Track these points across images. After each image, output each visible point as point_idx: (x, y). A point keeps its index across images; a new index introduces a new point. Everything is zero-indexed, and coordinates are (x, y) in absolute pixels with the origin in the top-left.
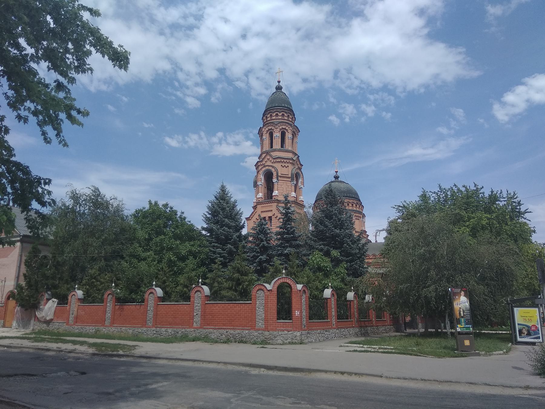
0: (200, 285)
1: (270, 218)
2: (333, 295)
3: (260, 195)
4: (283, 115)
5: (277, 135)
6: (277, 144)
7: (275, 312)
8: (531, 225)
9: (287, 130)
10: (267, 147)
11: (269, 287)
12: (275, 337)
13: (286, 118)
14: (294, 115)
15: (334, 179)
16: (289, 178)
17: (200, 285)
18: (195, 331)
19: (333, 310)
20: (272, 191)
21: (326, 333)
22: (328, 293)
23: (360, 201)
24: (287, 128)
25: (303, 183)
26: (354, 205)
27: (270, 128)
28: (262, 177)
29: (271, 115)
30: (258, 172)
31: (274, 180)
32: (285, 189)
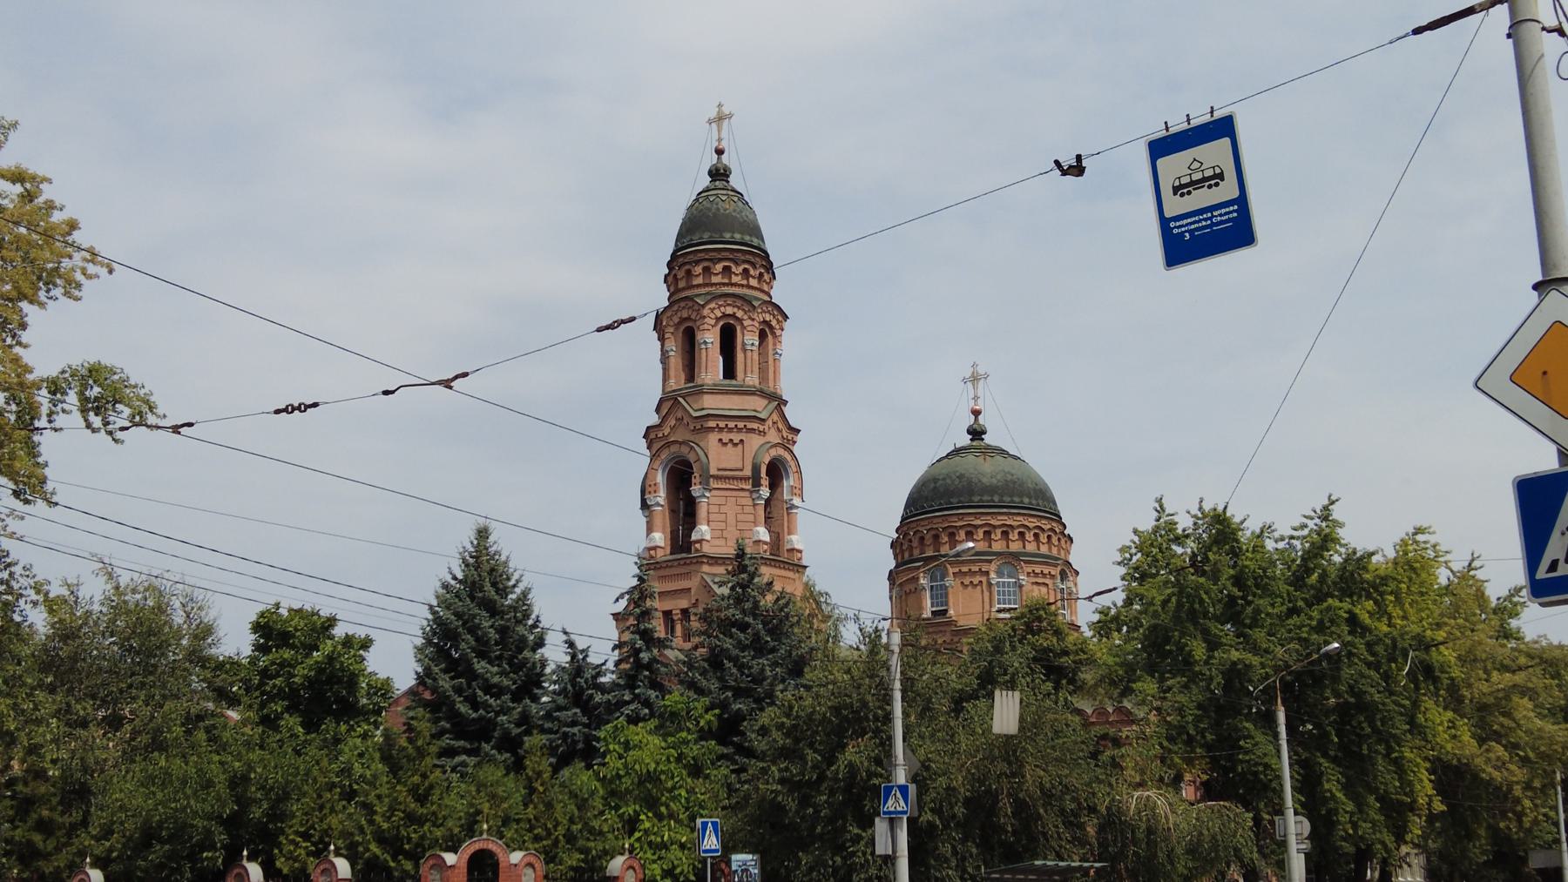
1: (685, 612)
5: (710, 338)
6: (712, 368)
8: (382, 675)
11: (450, 858)
15: (965, 440)
23: (1057, 518)
29: (707, 270)
31: (696, 490)
32: (731, 520)
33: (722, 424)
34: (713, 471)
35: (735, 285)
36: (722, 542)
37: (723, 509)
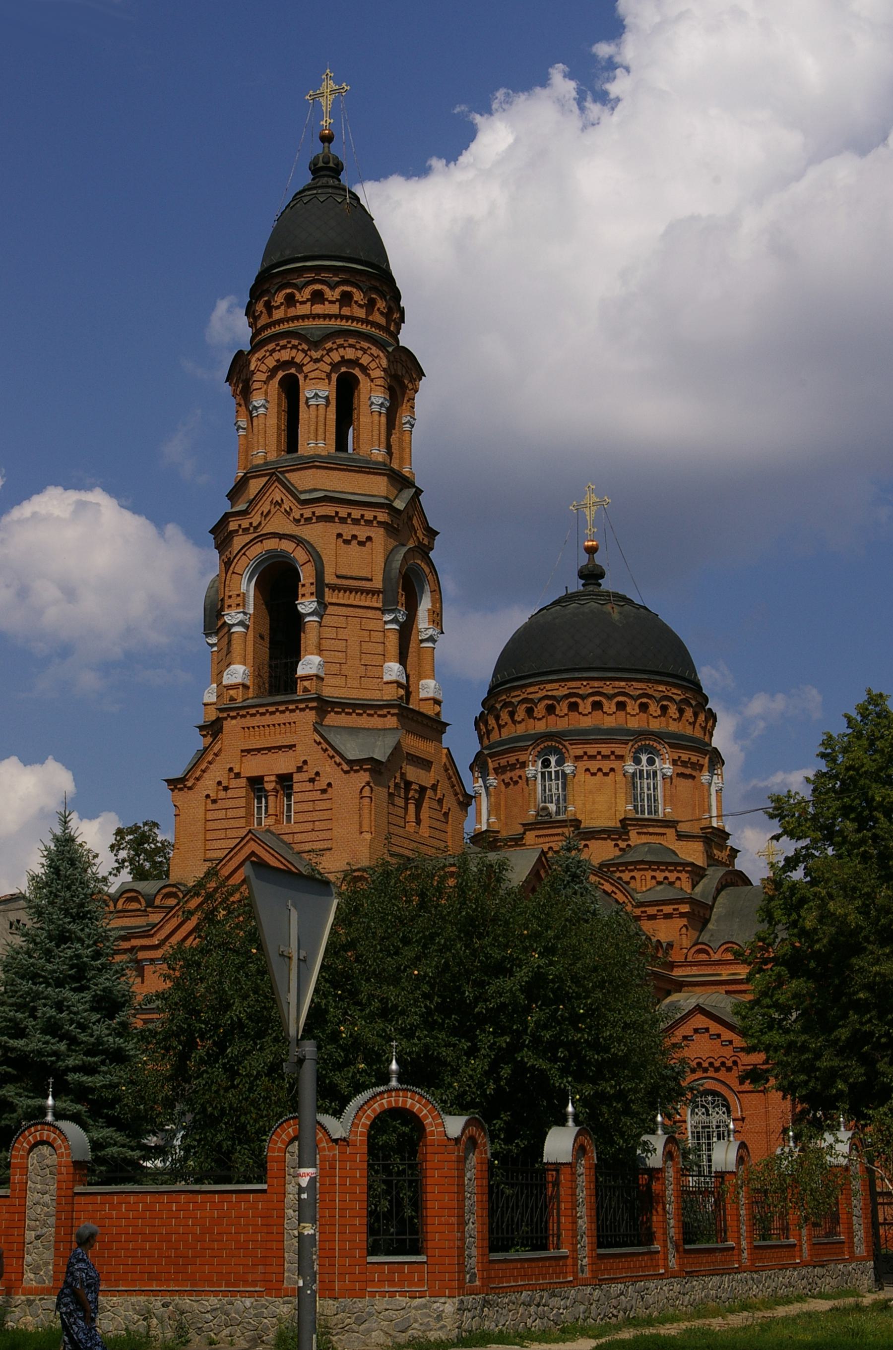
0: (50, 1118)
2: (580, 1150)
3: (237, 673)
4: (346, 299)
5: (317, 392)
6: (316, 440)
7: (360, 1222)
9: (364, 369)
10: (267, 448)
11: (336, 1127)
12: (360, 1321)
13: (361, 313)
15: (576, 585)
16: (373, 592)
17: (50, 1118)
18: (30, 1303)
19: (582, 1211)
20: (295, 655)
21: (554, 1301)
22: (559, 1144)
23: (696, 688)
24: (365, 360)
25: (436, 617)
26: (673, 710)
27: (285, 355)
28: (247, 587)
30: (227, 564)
31: (306, 605)
33: (343, 513)
34: (329, 578)
35: (353, 319)
36: (340, 681)
37: (342, 634)
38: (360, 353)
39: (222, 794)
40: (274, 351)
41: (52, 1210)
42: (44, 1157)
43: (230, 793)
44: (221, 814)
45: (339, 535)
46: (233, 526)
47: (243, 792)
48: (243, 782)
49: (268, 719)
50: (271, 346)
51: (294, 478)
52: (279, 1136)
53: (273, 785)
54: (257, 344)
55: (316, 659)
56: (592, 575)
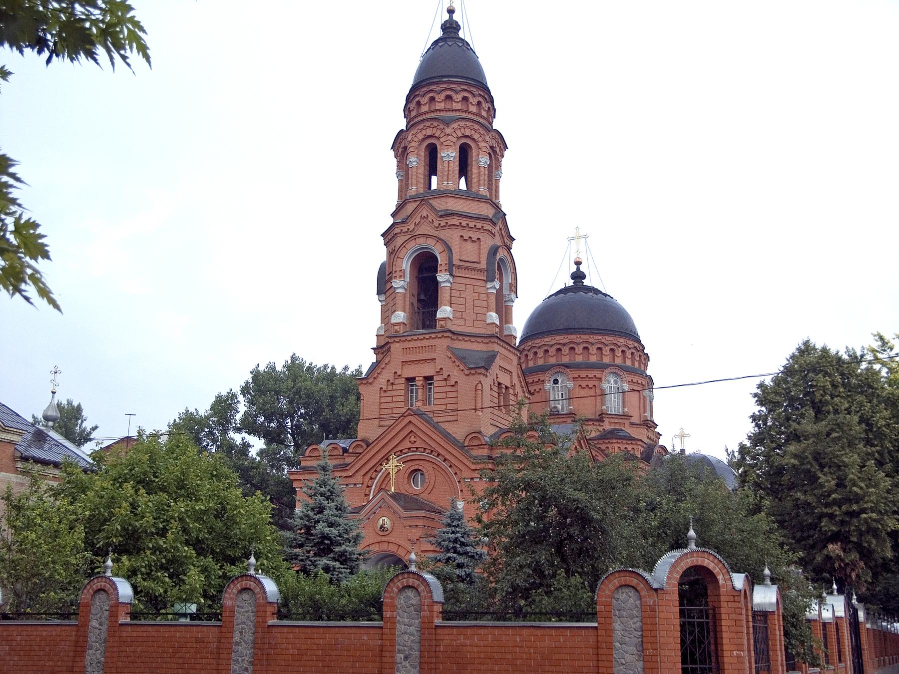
14: (492, 101)
15: (570, 283)
16: (480, 270)
23: (639, 341)
27: (429, 132)
28: (406, 265)
31: (442, 277)
34: (456, 262)
36: (462, 322)
38: (473, 132)
39: (390, 388)
40: (422, 129)
41: (417, 638)
42: (409, 598)
43: (395, 387)
44: (389, 399)
45: (462, 236)
46: (397, 230)
47: (403, 387)
48: (403, 381)
49: (418, 344)
50: (421, 126)
51: (434, 202)
52: (607, 586)
53: (421, 383)
54: (413, 125)
55: (448, 308)
56: (578, 276)
